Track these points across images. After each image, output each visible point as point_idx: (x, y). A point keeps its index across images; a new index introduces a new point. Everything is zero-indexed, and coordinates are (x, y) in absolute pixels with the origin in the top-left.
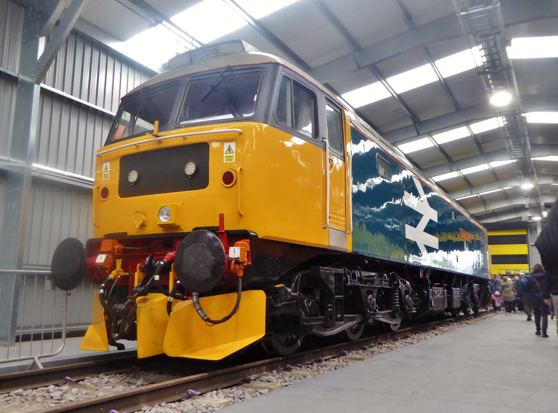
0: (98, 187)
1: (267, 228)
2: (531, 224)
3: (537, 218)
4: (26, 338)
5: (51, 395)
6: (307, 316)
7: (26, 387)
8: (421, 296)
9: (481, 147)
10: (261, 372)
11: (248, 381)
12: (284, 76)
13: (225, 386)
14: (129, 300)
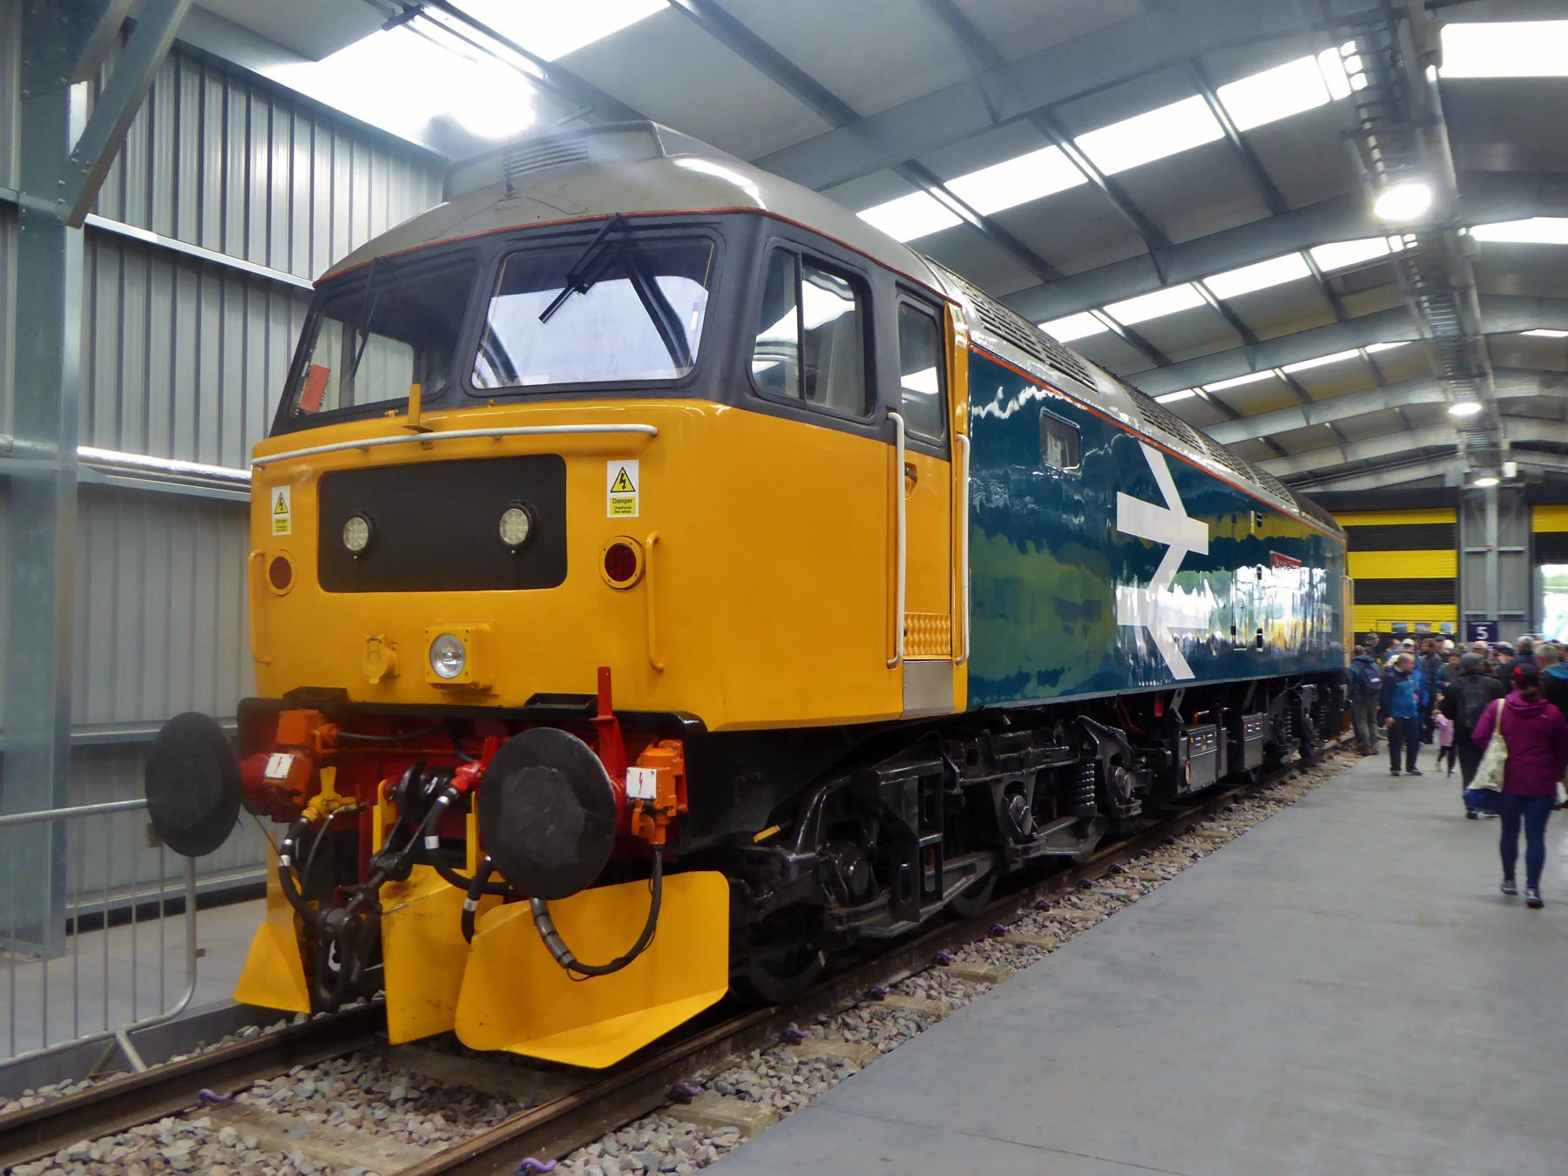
0: (263, 555)
1: (727, 702)
2: (1471, 495)
3: (1487, 482)
4: (90, 923)
5: (166, 1152)
6: (843, 904)
7: (96, 1130)
8: (1156, 762)
10: (720, 1057)
11: (683, 1098)
12: (778, 248)
13: (624, 1121)
14: (361, 896)
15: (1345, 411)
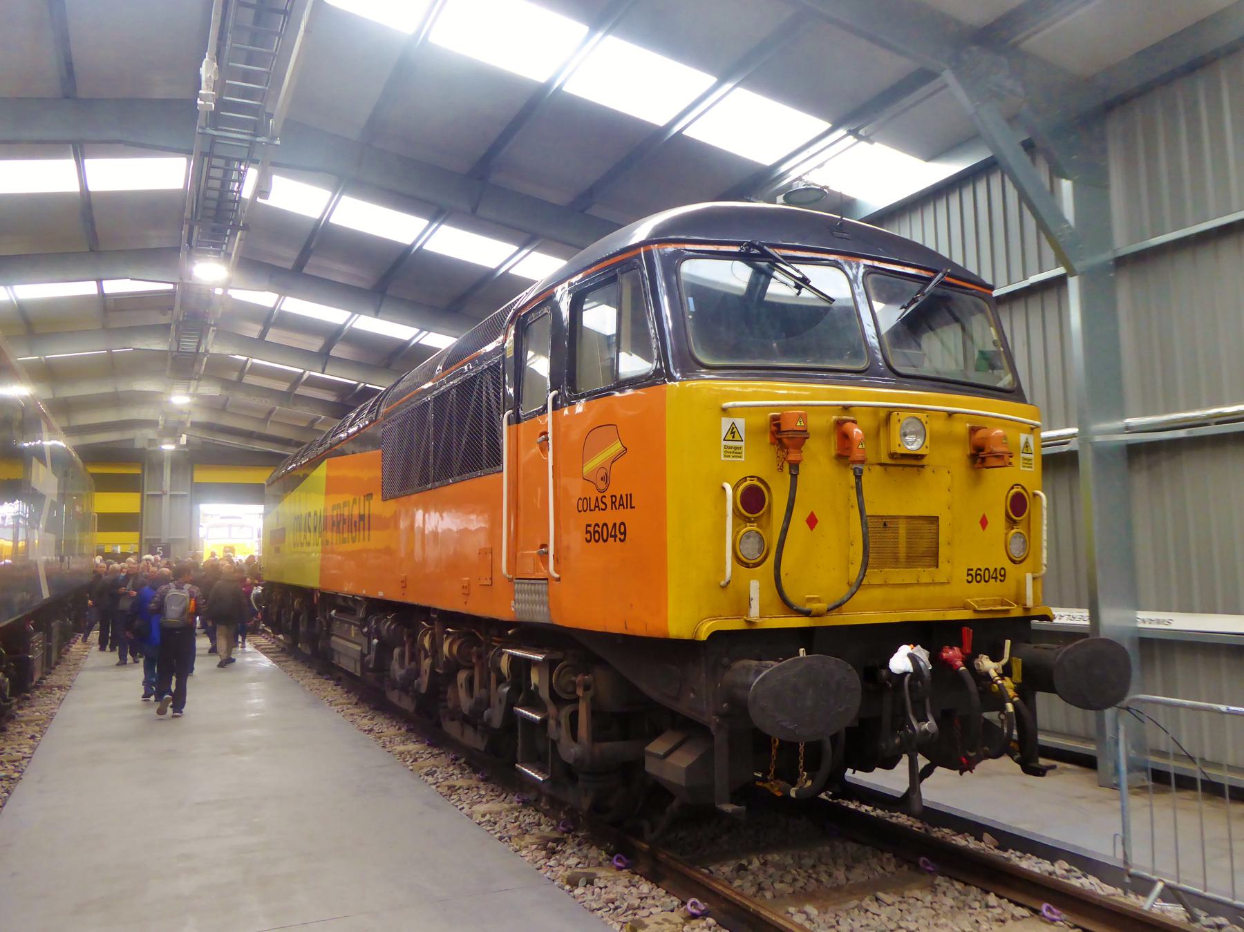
3: (168, 447)
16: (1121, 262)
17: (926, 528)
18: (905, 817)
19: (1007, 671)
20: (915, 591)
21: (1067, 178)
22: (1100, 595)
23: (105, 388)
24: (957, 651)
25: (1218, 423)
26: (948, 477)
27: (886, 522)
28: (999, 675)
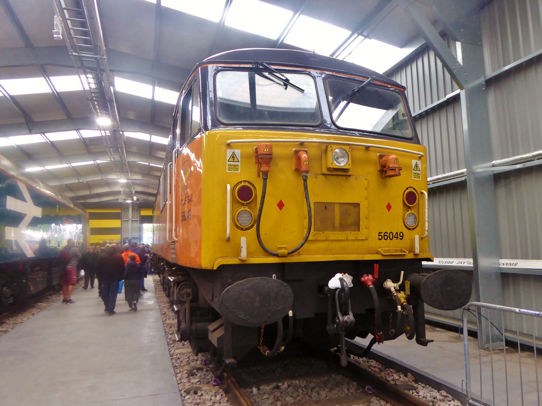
3: (129, 201)
9: (88, 147)
15: (90, 179)
16: (490, 83)
17: (352, 209)
18: (374, 362)
19: (402, 288)
20: (346, 244)
21: (458, 41)
22: (478, 250)
23: (98, 178)
24: (370, 277)
25: (538, 159)
26: (366, 182)
27: (326, 206)
28: (396, 290)
